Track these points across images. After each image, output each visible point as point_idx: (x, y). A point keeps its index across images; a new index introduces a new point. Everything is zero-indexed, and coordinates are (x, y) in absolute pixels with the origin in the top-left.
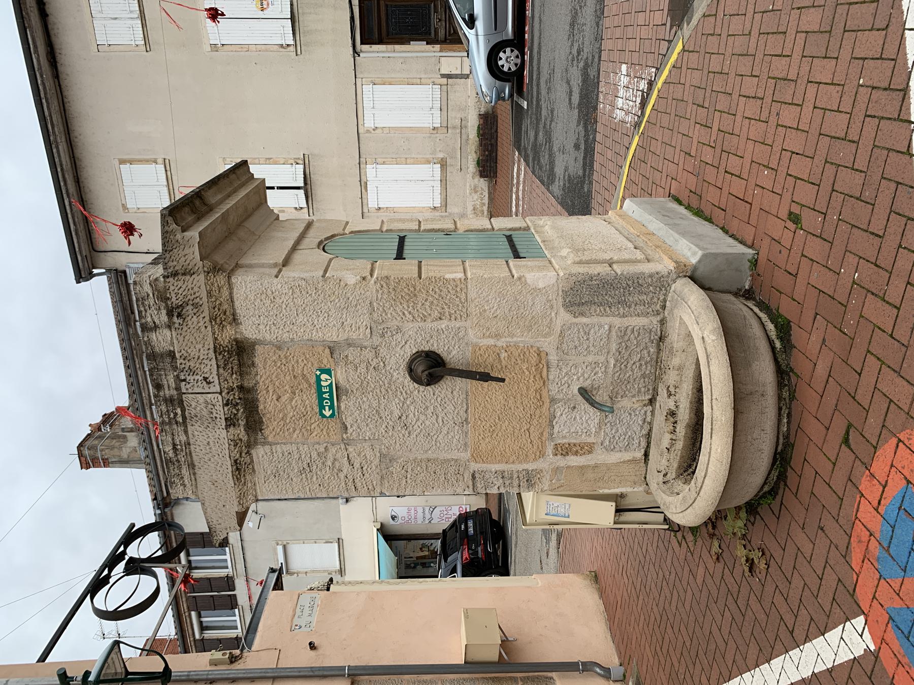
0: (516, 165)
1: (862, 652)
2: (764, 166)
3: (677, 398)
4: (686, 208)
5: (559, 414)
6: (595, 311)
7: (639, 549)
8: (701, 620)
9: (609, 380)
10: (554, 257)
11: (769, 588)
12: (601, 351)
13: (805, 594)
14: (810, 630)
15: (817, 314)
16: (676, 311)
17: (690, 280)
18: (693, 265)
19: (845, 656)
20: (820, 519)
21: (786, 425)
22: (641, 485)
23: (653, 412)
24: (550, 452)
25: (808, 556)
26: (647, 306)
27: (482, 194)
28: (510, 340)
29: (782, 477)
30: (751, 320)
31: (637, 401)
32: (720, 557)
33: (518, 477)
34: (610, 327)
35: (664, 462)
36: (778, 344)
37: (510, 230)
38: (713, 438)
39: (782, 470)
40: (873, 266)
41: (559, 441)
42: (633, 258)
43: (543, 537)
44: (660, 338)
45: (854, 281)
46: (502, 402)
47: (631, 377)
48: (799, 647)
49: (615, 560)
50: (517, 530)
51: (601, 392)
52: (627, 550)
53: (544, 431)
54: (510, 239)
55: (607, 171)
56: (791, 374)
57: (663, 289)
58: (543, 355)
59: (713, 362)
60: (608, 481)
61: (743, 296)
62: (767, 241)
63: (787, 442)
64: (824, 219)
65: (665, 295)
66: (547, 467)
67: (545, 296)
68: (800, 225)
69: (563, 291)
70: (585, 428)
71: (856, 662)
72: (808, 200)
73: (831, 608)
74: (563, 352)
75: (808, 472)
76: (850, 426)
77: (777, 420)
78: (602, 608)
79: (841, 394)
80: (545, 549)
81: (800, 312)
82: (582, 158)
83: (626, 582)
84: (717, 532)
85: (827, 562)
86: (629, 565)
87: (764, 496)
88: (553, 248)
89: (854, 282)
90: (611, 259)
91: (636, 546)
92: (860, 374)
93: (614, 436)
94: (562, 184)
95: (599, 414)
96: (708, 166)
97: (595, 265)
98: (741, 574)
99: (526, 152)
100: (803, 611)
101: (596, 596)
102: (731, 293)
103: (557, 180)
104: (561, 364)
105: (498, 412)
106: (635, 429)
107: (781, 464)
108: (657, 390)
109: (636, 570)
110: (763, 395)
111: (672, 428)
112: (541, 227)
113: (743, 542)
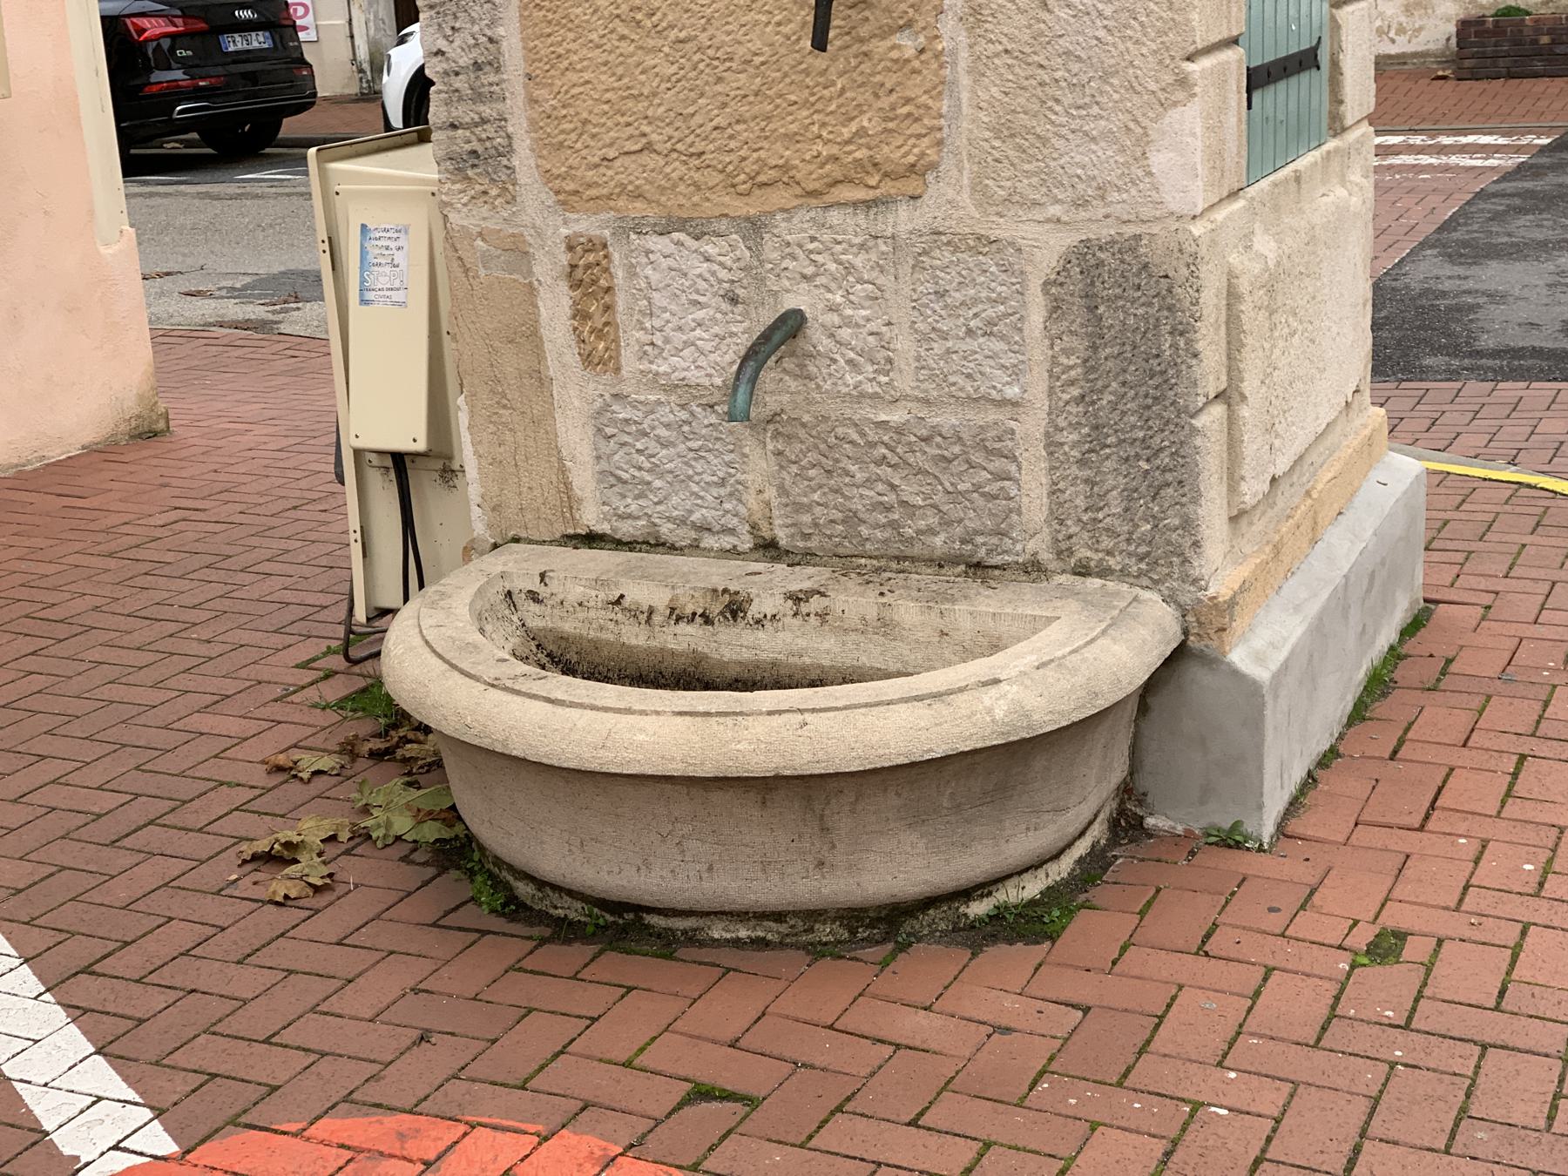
0: (1502, 141)
1: (67, 1151)
2: (1550, 861)
3: (788, 620)
4: (1392, 648)
5: (711, 250)
6: (1067, 352)
7: (269, 554)
8: (76, 729)
9: (833, 409)
10: (1251, 210)
11: (216, 911)
12: (932, 378)
13: (215, 1001)
14: (105, 1018)
15: (1086, 1010)
16: (1073, 605)
17: (1175, 645)
18: (1224, 654)
19: (46, 1109)
20: (453, 1034)
21: (728, 936)
22: (490, 526)
23: (733, 553)
24: (577, 228)
25: (334, 1004)
26: (1085, 518)
27: (1401, 30)
28: (963, 65)
29: (565, 931)
30: (1052, 827)
31: (768, 504)
32: (281, 777)
33: (484, 121)
34: (1015, 404)
35: (576, 592)
36: (978, 908)
37: (1335, 65)
38: (679, 719)
39: (590, 929)
40: (1254, 1152)
41: (616, 256)
42: (1246, 470)
43: (248, 279)
44: (978, 565)
45: (1202, 1104)
46: (741, 51)
47: (847, 480)
48: (48, 990)
49: (218, 487)
50: (257, 196)
51: (793, 384)
52: (257, 520)
53: (649, 202)
54: (1306, 61)
55: (1498, 422)
56: (890, 946)
57: (1143, 566)
58: (912, 186)
59: (919, 715)
60: (494, 423)
61: (1122, 811)
62: (1308, 875)
63: (677, 941)
64: (1390, 1025)
65: (1124, 574)
66: (526, 219)
67: (1119, 177)
68: (1365, 961)
69: (1138, 238)
70: (667, 341)
71: (37, 1136)
72: (1446, 980)
73: (185, 1070)
74: (925, 253)
75: (589, 999)
76: (751, 1102)
77: (743, 908)
78: (56, 454)
79: (846, 1078)
80: (211, 287)
81: (1089, 966)
82: (1537, 344)
83: (152, 521)
84: (362, 764)
85: (323, 1055)
86: (210, 527)
87: (497, 884)
88: (1276, 208)
89: (1197, 1106)
90: (1243, 398)
91: (275, 544)
92: (913, 1123)
93: (646, 434)
94: (1447, 285)
95: (718, 381)
96: (1538, 707)
97: (1223, 344)
98: (243, 833)
99: (1553, 168)
100: (160, 999)
101: (90, 435)
102: (1131, 774)
103: (1460, 270)
104: (884, 248)
105: (703, 37)
106: (675, 500)
107: (606, 927)
108: (808, 564)
109: (200, 547)
110: (821, 864)
111: (688, 611)
112: (1343, 176)
113: (344, 836)
